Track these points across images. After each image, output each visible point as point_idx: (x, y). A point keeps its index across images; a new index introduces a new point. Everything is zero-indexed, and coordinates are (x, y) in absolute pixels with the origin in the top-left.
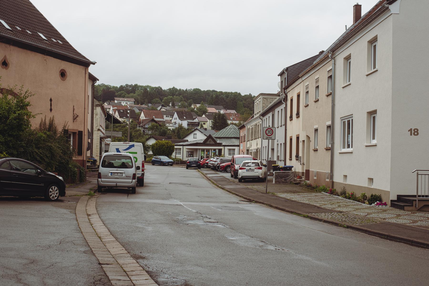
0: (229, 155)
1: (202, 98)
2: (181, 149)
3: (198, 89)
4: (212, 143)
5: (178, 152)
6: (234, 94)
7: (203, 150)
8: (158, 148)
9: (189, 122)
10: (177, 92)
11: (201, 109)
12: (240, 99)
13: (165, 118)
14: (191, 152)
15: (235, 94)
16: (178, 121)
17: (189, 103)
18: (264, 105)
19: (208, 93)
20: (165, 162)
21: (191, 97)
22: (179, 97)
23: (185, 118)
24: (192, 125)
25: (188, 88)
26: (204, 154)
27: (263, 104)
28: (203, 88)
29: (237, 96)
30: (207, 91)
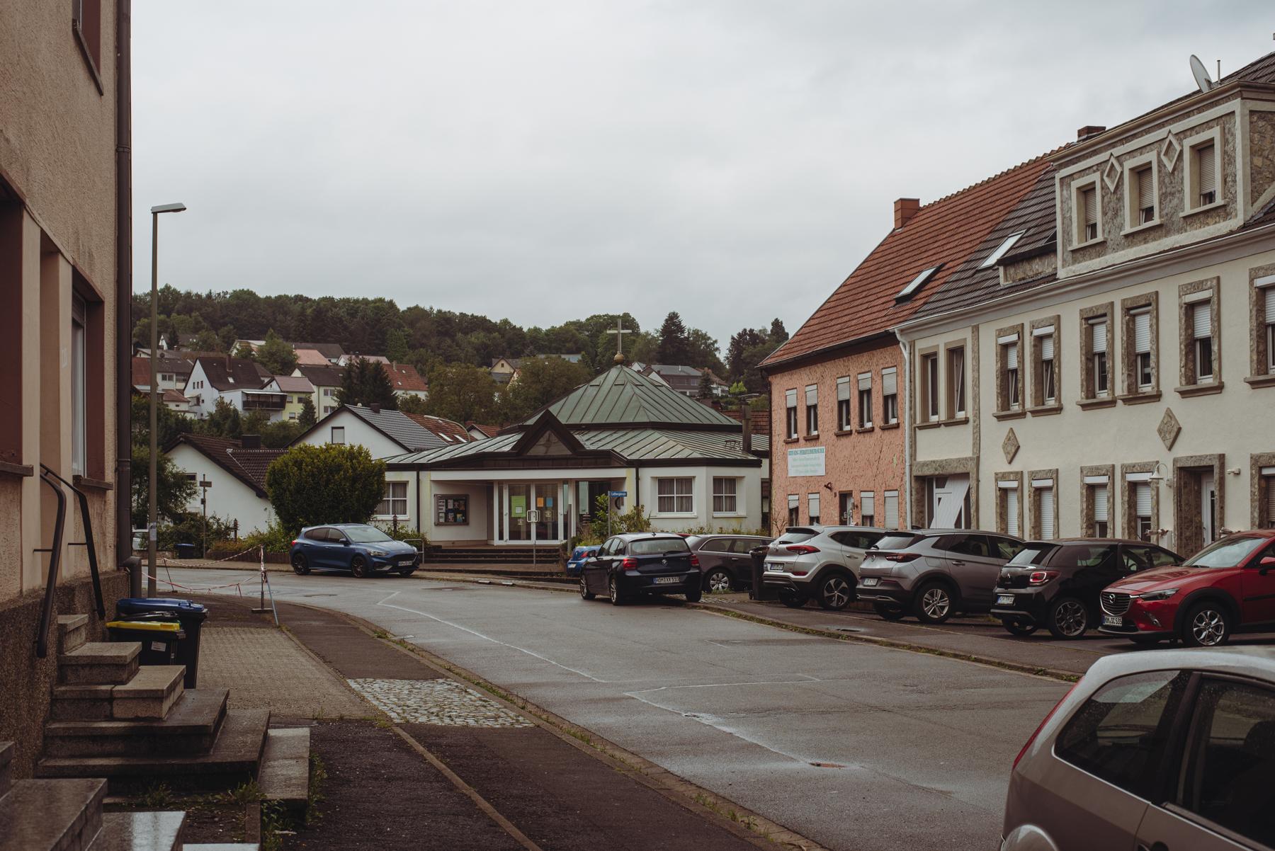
0: (660, 511)
1: (263, 320)
2: (404, 485)
3: (248, 290)
4: (561, 450)
5: (391, 499)
6: (372, 305)
7: (517, 488)
8: (306, 482)
9: (247, 395)
10: (180, 302)
11: (272, 354)
12: (394, 322)
13: (163, 385)
14: (456, 499)
15: (378, 304)
16: (210, 395)
17: (224, 337)
18: (1258, 161)
19: (281, 304)
20: (375, 556)
21: (226, 319)
22: (190, 317)
23: (231, 380)
24: (261, 404)
25: (216, 290)
26: (528, 506)
27: (1251, 154)
28: (265, 290)
29: (383, 309)
30: (280, 297)
